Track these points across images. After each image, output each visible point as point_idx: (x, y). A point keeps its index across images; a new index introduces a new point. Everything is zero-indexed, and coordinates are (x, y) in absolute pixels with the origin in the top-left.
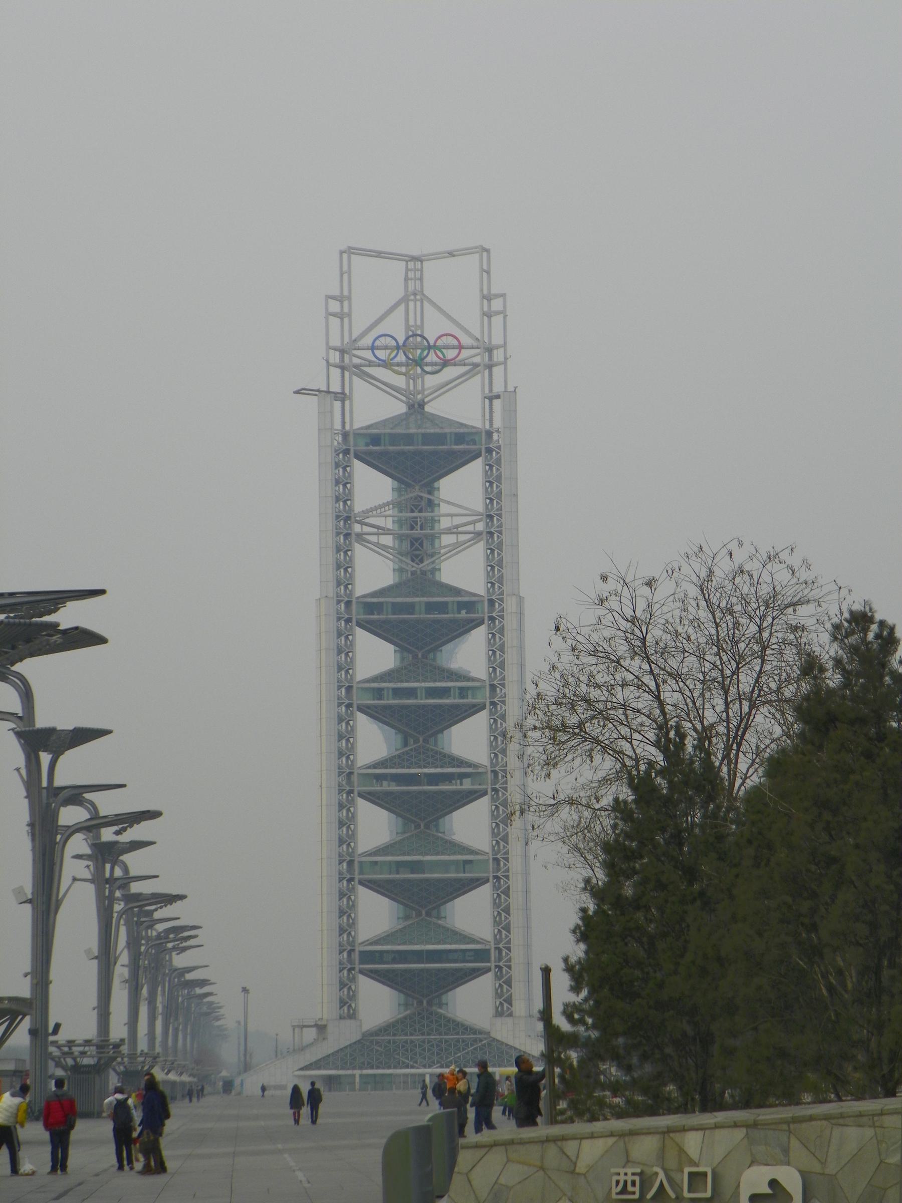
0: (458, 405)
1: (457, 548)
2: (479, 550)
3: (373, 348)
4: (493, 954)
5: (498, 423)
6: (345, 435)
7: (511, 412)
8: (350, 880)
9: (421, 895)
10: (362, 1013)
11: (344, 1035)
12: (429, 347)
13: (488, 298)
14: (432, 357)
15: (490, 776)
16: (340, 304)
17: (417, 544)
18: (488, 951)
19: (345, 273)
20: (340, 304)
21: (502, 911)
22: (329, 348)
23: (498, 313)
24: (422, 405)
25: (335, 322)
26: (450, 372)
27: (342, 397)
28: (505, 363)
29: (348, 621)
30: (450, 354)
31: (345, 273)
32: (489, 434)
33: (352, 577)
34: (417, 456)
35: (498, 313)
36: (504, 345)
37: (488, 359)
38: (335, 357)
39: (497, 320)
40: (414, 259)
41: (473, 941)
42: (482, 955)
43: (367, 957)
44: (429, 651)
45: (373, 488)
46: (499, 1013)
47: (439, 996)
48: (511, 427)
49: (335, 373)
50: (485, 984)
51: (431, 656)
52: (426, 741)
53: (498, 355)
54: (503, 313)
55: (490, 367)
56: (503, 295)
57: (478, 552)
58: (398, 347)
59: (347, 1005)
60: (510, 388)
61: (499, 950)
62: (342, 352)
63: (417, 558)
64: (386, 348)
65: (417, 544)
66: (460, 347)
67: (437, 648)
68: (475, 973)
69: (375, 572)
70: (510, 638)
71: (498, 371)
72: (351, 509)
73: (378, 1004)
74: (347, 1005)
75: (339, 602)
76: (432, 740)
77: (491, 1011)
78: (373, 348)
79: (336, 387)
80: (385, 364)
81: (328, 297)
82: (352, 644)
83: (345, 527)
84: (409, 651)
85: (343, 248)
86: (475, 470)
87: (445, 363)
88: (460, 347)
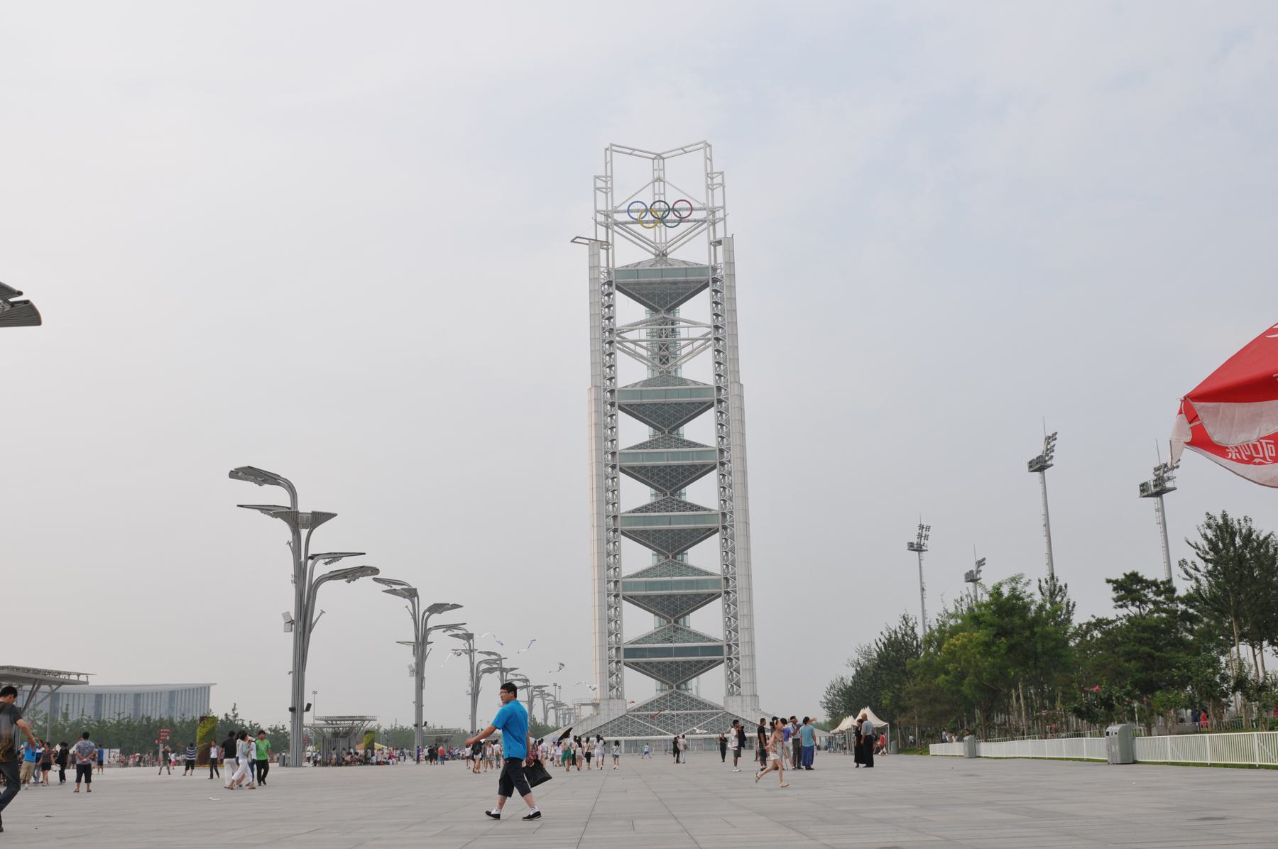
0: (693, 251)
1: (692, 354)
2: (708, 355)
3: (628, 211)
4: (726, 649)
5: (720, 259)
6: (609, 273)
7: (730, 252)
8: (617, 662)
9: (669, 480)
10: (628, 696)
11: (614, 711)
12: (669, 210)
13: (710, 175)
14: (671, 216)
15: (726, 649)
16: (604, 183)
17: (664, 352)
18: (721, 647)
19: (608, 163)
20: (604, 183)
21: (727, 551)
22: (597, 212)
23: (721, 220)
24: (665, 255)
25: (601, 195)
26: (684, 226)
27: (606, 245)
28: (724, 219)
29: (617, 596)
30: (684, 214)
31: (608, 163)
32: (714, 269)
33: (618, 497)
34: (662, 291)
35: (721, 220)
36: (724, 207)
37: (712, 218)
38: (601, 218)
39: (718, 192)
40: (659, 156)
41: (710, 640)
42: (717, 650)
43: (630, 653)
44: (678, 553)
45: (629, 311)
46: (730, 693)
47: (685, 683)
48: (730, 264)
49: (602, 230)
50: (718, 673)
51: (679, 557)
52: (674, 557)
53: (719, 214)
54: (722, 185)
55: (714, 224)
56: (722, 173)
57: (708, 356)
58: (646, 210)
59: (615, 688)
60: (729, 235)
61: (729, 646)
62: (607, 216)
63: (664, 360)
64: (638, 211)
65: (664, 352)
66: (692, 209)
67: (682, 552)
68: (711, 665)
69: (632, 372)
70: (739, 543)
71: (719, 226)
72: (618, 509)
73: (641, 688)
74: (615, 688)
75: (609, 582)
76: (681, 621)
77: (723, 692)
78: (628, 211)
79: (602, 237)
80: (637, 221)
81: (597, 177)
82: (619, 548)
83: (608, 338)
84: (659, 430)
85: (607, 145)
86: (705, 297)
87: (681, 220)
88: (692, 209)
